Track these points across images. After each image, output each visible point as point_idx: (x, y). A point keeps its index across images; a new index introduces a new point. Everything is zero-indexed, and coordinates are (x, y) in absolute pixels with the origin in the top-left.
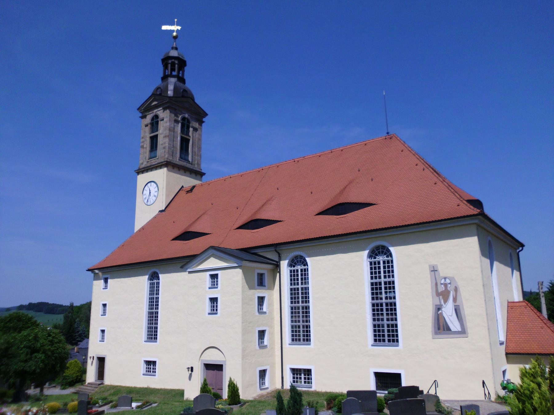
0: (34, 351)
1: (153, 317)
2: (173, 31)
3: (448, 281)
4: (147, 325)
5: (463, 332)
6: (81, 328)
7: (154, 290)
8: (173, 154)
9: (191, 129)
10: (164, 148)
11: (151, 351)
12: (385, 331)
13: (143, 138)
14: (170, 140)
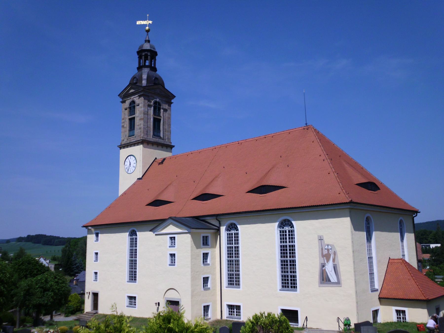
0: (46, 290)
1: (133, 264)
2: (145, 25)
3: (330, 247)
4: (129, 269)
5: (338, 283)
6: (78, 261)
7: (133, 243)
8: (147, 133)
9: (162, 111)
10: (140, 128)
11: (132, 289)
12: (289, 281)
13: (123, 119)
14: (144, 122)
